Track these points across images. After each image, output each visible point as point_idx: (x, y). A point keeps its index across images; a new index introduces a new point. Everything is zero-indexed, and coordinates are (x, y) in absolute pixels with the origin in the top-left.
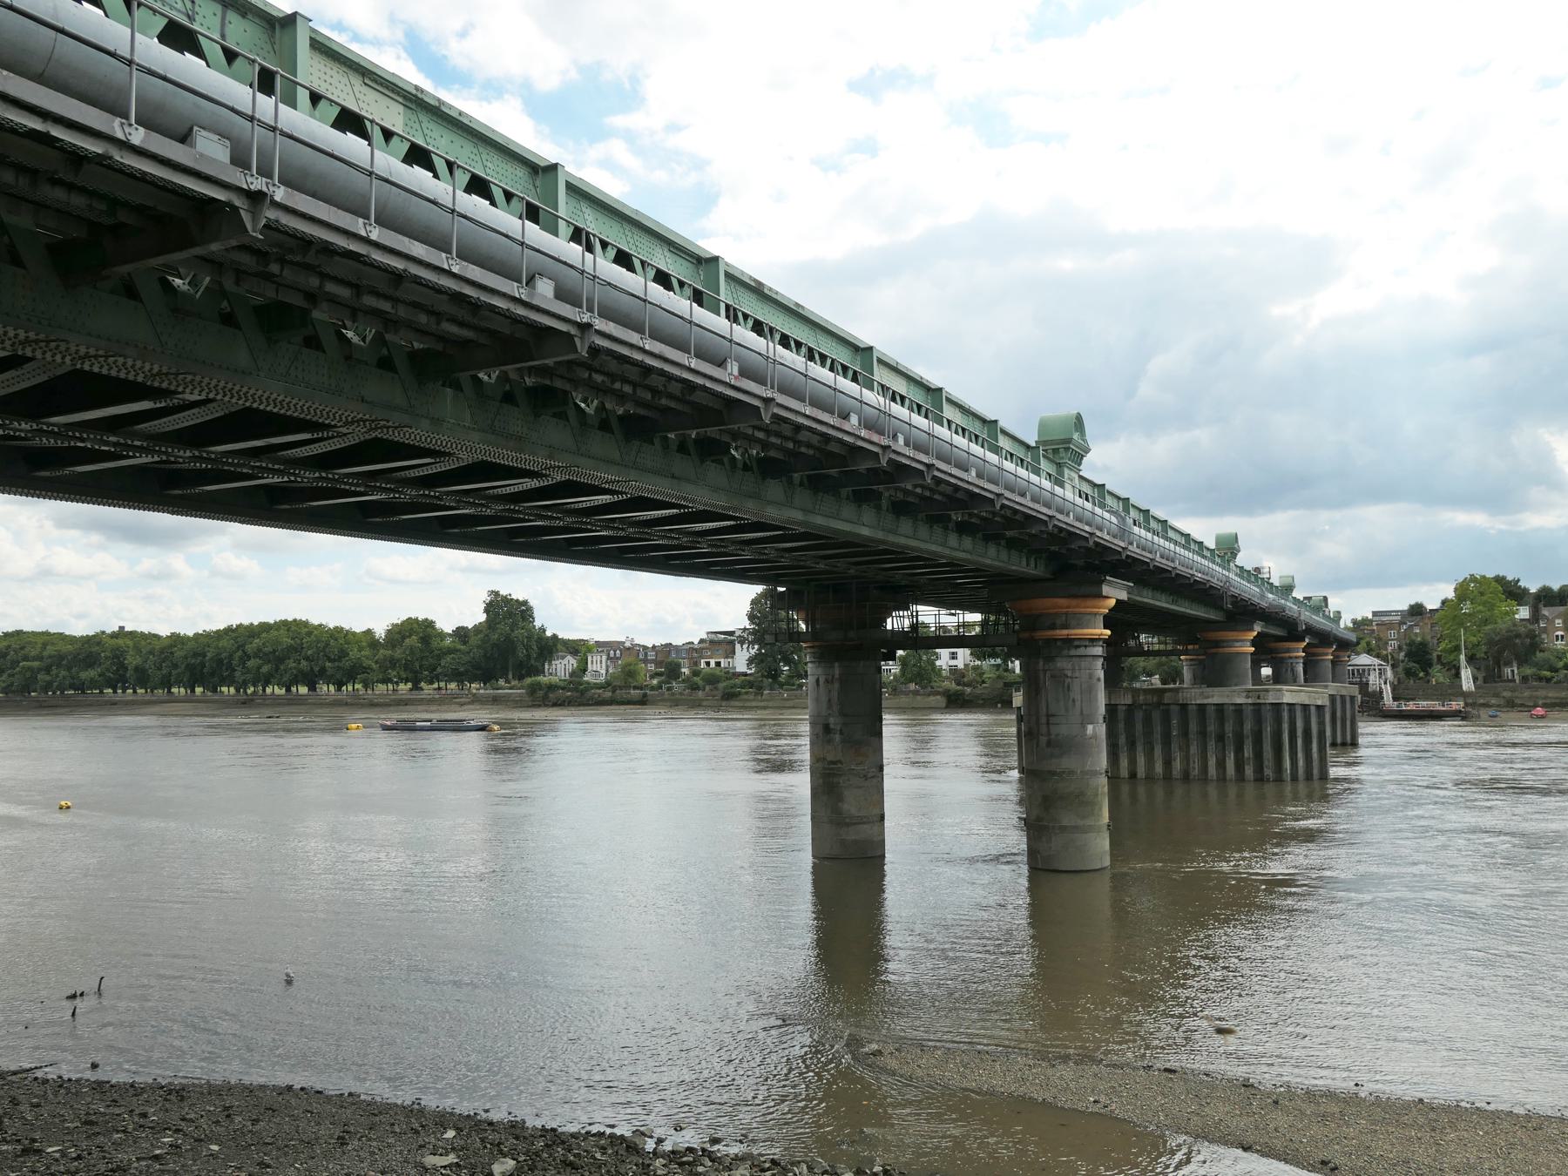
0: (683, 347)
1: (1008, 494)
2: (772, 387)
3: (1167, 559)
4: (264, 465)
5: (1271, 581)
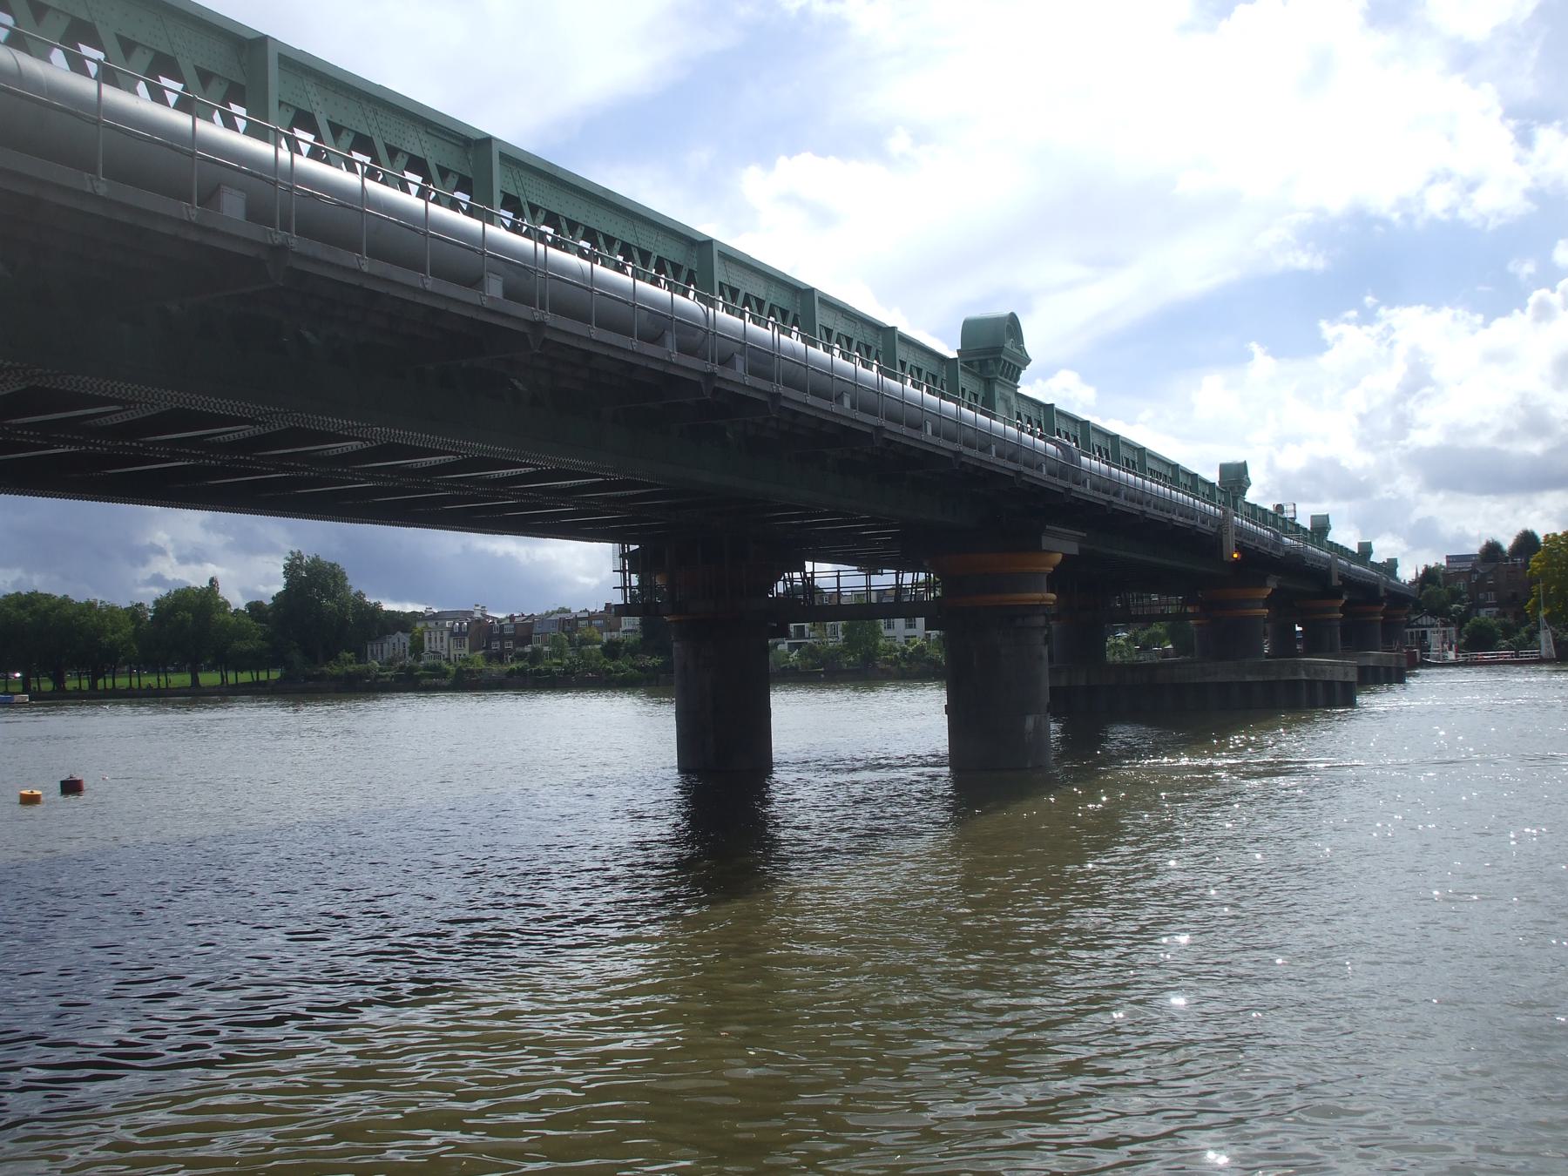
0: (585, 319)
1: (966, 451)
2: (713, 361)
3: (1162, 510)
4: (187, 451)
5: (1297, 521)
